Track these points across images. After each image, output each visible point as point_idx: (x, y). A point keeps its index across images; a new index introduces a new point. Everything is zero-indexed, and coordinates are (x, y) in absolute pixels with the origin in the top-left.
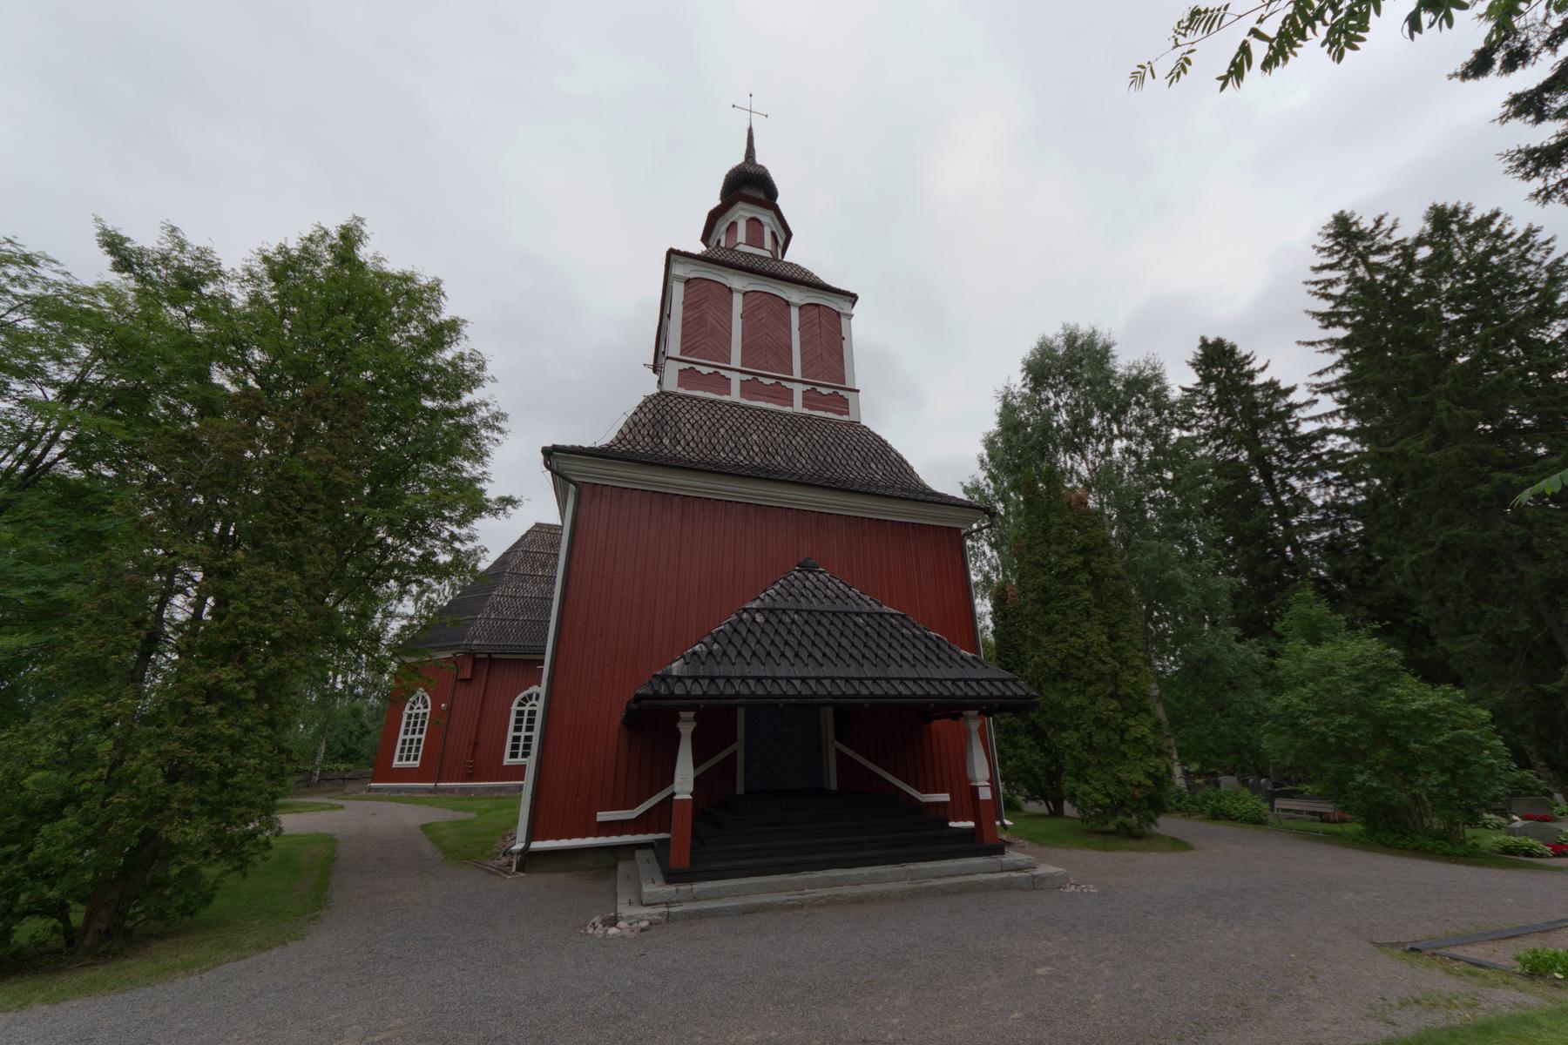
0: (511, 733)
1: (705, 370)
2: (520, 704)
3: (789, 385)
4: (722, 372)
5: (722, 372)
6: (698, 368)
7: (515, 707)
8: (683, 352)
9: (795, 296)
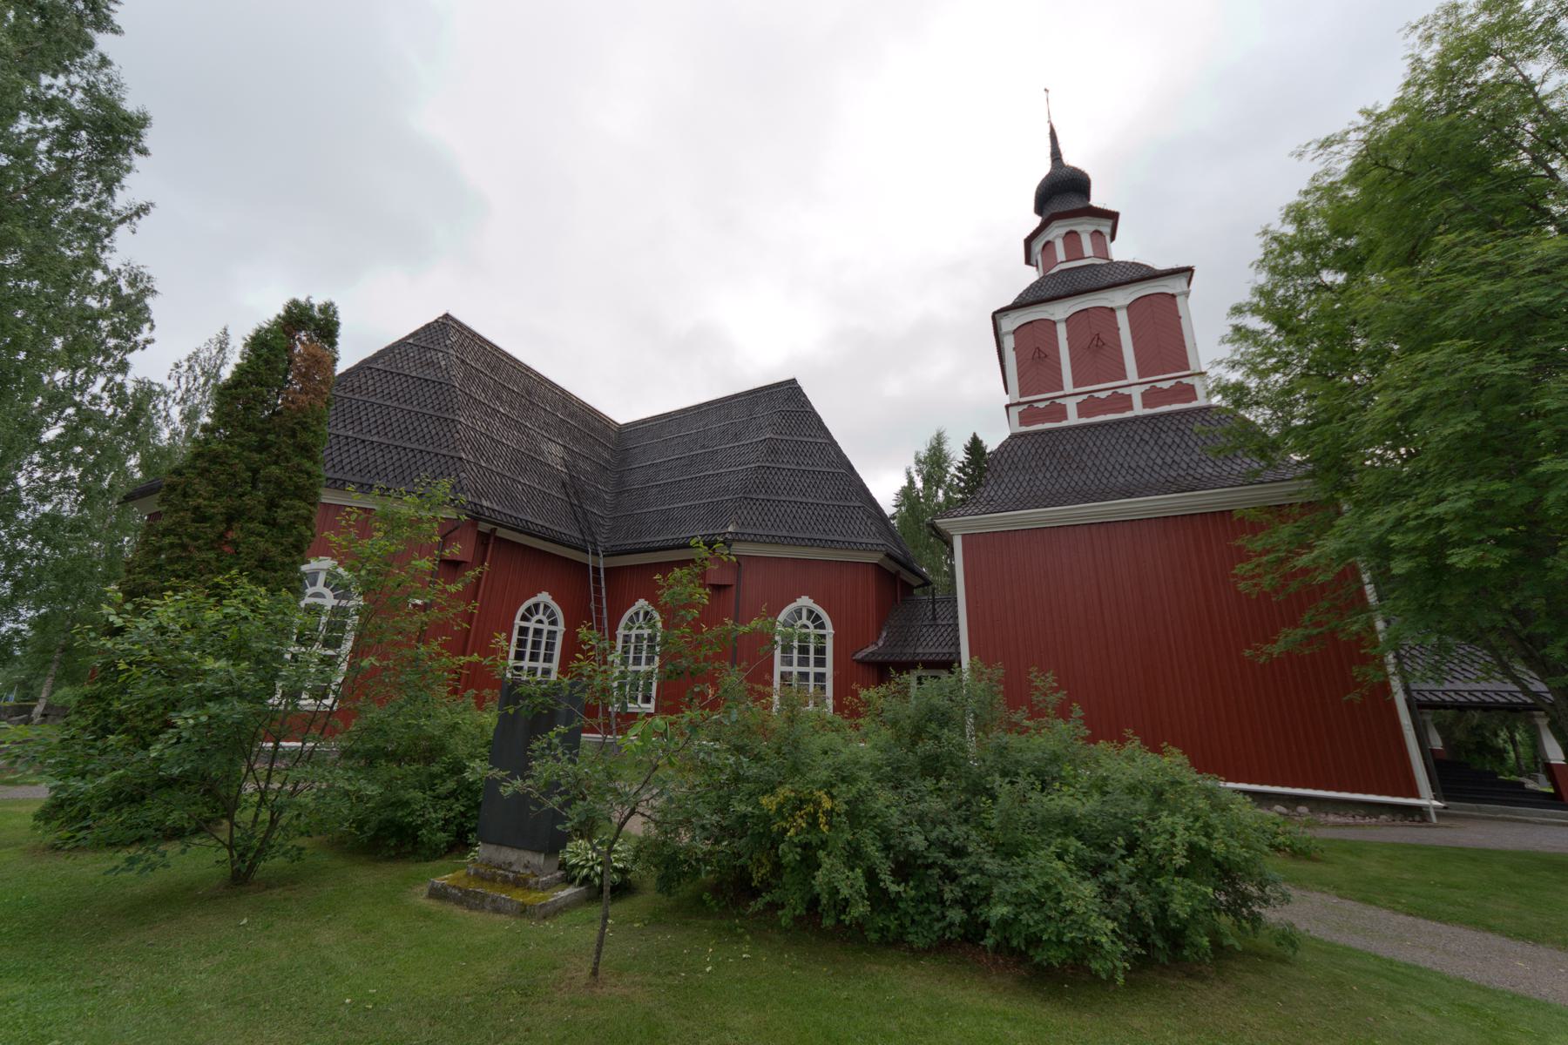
0: (828, 670)
1: (1166, 385)
2: (524, 618)
3: (1126, 391)
4: (1185, 381)
5: (1185, 381)
6: (1159, 385)
7: (518, 622)
8: (1076, 385)
9: (1119, 299)
